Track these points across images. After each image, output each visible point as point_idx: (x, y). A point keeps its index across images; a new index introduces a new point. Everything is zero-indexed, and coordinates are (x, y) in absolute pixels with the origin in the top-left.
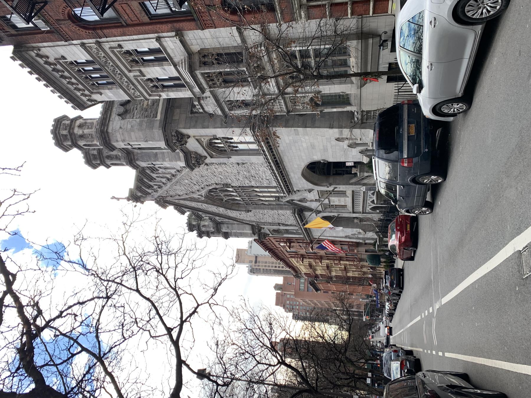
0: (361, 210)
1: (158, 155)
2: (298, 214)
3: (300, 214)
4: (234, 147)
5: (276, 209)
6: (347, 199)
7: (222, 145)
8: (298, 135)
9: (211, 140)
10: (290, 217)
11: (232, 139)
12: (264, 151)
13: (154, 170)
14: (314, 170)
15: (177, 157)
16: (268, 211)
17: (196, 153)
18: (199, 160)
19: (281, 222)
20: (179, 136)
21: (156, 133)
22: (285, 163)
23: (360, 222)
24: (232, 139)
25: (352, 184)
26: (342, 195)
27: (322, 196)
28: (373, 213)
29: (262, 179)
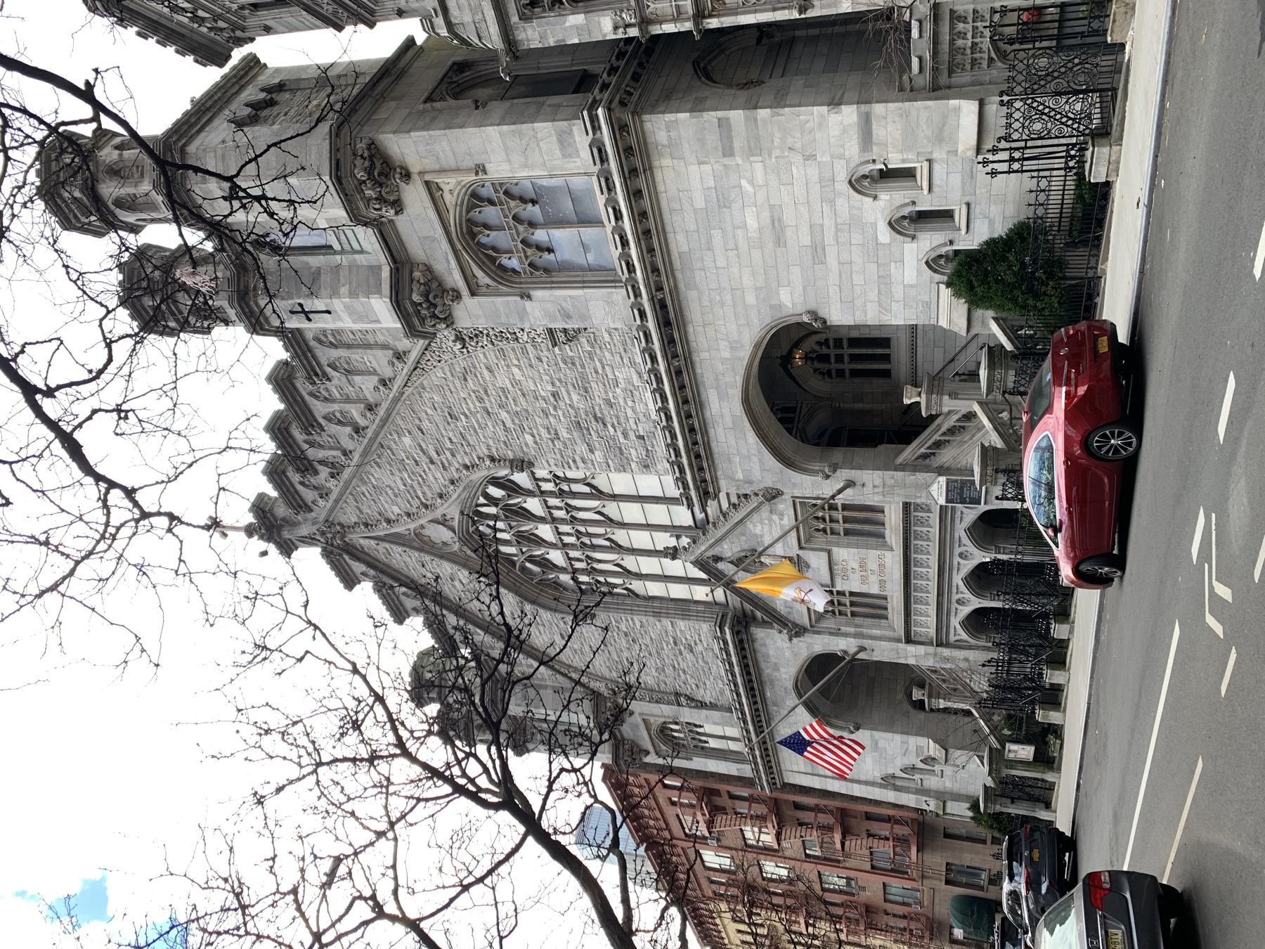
0: (932, 632)
1: (323, 277)
2: (731, 629)
3: (738, 633)
4: (700, 741)
5: (667, 615)
6: (888, 554)
7: (682, 735)
8: (732, 154)
9: (665, 723)
10: (709, 657)
11: (700, 726)
12: (754, 757)
13: (317, 375)
14: (790, 426)
15: (372, 281)
16: (644, 619)
17: (428, 269)
18: (435, 297)
19: (683, 691)
20: (378, 165)
21: (314, 150)
22: (690, 329)
23: (930, 696)
24: (700, 726)
25: (902, 468)
26: (872, 541)
27: (808, 541)
28: (970, 648)
29: (625, 435)
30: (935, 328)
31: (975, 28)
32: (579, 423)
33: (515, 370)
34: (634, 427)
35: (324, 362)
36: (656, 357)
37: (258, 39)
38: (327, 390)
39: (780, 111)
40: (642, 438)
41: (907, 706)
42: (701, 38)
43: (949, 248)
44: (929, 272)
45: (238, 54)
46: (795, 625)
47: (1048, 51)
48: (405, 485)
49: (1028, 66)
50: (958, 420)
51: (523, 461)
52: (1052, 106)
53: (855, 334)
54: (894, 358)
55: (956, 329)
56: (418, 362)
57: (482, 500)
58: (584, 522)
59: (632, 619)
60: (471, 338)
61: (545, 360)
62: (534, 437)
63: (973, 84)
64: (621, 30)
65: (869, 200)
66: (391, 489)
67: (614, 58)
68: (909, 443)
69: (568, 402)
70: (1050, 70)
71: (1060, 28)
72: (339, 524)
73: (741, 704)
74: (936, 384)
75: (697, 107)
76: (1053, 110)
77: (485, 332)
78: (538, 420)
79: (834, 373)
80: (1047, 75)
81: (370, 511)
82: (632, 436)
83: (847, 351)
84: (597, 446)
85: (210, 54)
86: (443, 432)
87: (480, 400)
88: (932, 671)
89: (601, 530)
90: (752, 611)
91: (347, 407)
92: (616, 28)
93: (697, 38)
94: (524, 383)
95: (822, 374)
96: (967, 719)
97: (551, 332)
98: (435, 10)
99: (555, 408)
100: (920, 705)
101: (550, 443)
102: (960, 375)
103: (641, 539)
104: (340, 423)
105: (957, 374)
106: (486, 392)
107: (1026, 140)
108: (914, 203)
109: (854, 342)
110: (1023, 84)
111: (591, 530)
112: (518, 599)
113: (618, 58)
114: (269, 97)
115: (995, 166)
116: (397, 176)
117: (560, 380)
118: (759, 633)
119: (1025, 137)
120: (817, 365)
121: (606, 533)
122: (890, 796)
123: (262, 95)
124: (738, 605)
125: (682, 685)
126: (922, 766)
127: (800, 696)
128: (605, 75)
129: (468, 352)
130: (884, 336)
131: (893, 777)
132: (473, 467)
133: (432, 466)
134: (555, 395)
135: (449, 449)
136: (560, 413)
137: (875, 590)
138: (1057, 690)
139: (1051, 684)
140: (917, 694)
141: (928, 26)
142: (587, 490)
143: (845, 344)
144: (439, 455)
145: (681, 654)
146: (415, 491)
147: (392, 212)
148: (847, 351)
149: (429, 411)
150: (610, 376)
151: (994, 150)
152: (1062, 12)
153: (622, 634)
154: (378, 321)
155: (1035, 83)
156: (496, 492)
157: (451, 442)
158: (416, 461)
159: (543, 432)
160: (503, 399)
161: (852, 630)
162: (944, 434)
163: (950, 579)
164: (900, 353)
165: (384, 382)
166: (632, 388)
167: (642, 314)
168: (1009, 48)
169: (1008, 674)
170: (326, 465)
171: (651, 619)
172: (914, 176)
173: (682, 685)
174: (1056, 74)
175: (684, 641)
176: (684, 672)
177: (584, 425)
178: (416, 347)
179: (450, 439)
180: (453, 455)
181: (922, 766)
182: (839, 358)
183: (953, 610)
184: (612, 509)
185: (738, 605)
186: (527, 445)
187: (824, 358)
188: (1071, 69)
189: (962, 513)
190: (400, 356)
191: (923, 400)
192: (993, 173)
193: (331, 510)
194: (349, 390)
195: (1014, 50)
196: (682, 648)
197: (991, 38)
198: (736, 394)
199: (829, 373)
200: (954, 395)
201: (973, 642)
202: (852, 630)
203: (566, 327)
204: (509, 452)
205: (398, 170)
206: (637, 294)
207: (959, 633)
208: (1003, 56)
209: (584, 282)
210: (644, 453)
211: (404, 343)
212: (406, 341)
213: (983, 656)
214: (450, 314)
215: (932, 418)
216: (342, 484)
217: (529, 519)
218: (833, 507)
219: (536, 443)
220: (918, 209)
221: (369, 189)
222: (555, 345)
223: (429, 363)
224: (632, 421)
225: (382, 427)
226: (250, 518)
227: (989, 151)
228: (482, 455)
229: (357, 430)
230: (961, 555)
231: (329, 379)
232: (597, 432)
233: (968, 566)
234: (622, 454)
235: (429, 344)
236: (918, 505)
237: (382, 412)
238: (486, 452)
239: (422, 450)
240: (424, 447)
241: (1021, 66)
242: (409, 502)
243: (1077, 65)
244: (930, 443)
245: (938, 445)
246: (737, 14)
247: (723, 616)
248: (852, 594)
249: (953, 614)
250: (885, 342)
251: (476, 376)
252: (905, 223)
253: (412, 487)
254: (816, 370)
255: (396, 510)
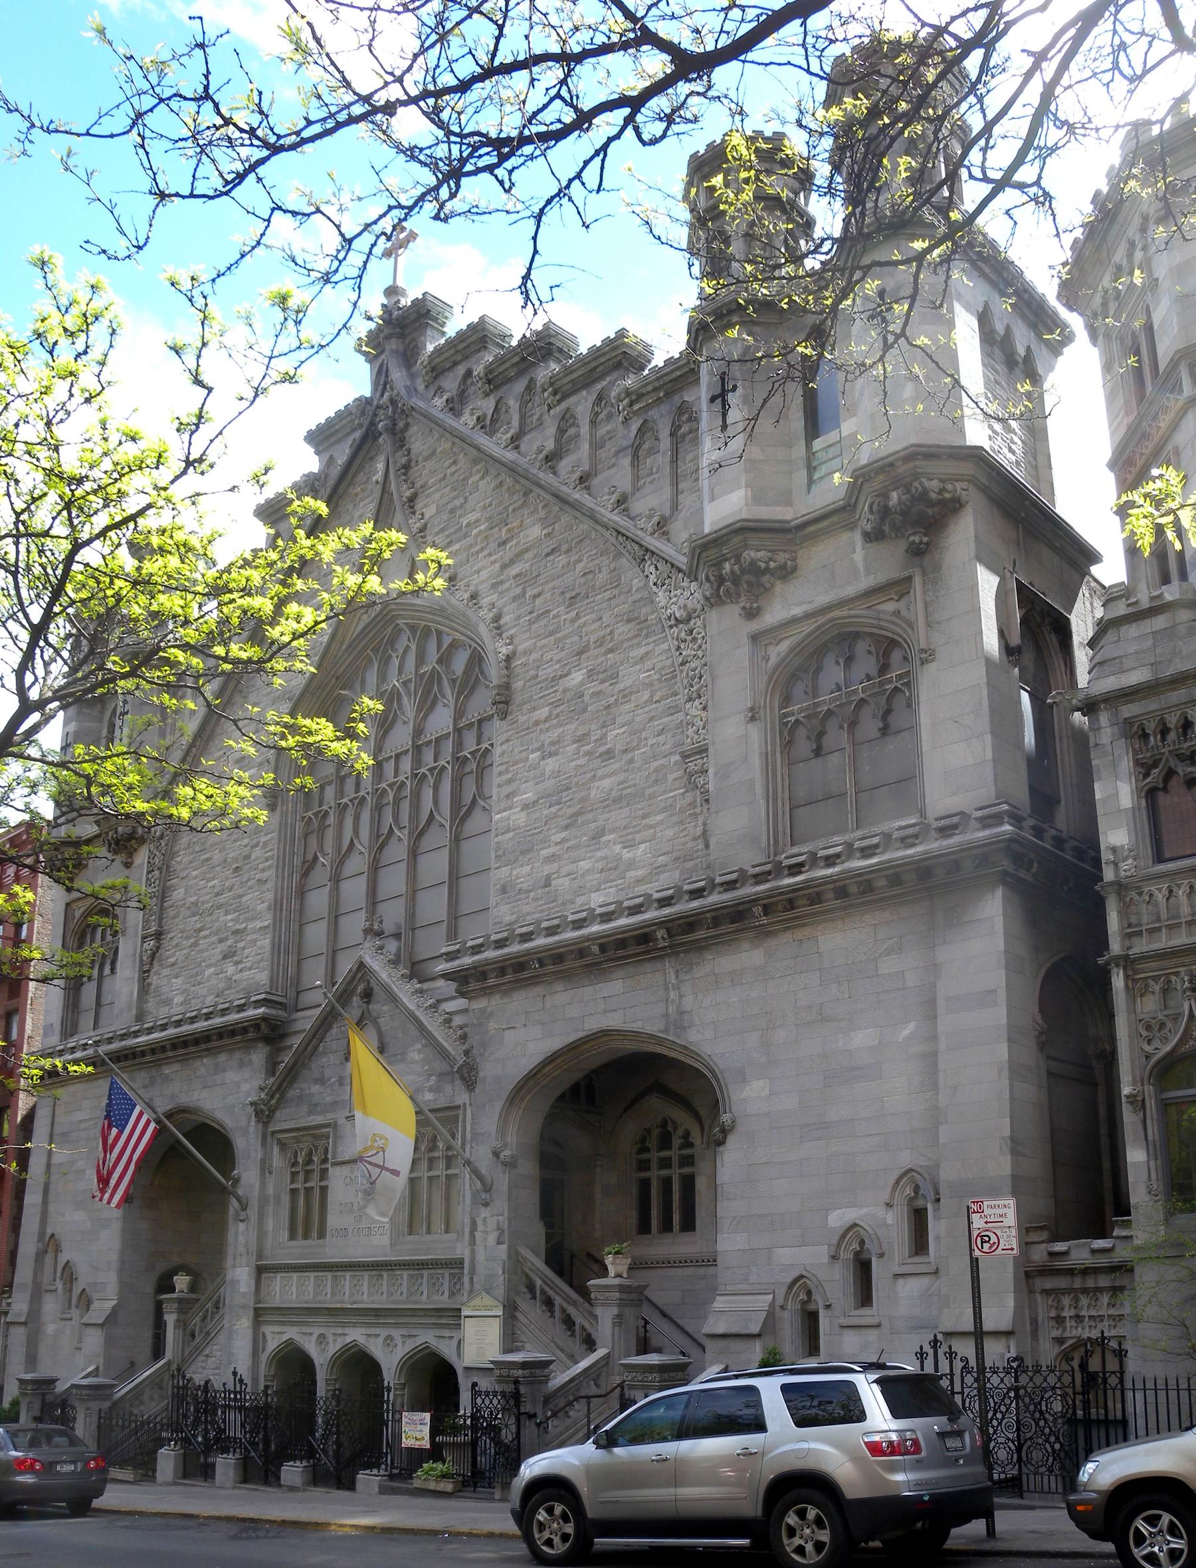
0: (276, 1302)
2: (264, 1018)
5: (277, 921)
6: (385, 1240)
16: (270, 885)
23: (180, 1301)
28: (255, 1354)
30: (713, 1291)
31: (1101, 1318)
32: (568, 789)
33: (646, 695)
34: (564, 871)
35: (653, 413)
36: (669, 905)
37: (1096, 350)
38: (610, 416)
39: (1006, 1073)
40: (547, 884)
41: (162, 1267)
42: (1100, 966)
43: (821, 1305)
44: (789, 1280)
45: (1075, 321)
46: (273, 1111)
47: (1071, 1411)
48: (468, 525)
49: (1054, 1388)
50: (583, 1328)
51: (507, 703)
52: (1004, 1422)
53: (701, 1184)
54: (667, 1238)
55: (711, 1319)
56: (653, 553)
57: (447, 641)
58: (416, 797)
59: (270, 867)
60: (691, 631)
61: (662, 738)
62: (546, 721)
63: (1034, 1322)
64: (1112, 857)
65: (885, 1195)
66: (462, 506)
67: (1076, 843)
68: (547, 1263)
69: (599, 773)
70: (1047, 1416)
71: (1098, 1421)
72: (407, 425)
73: (150, 1031)
74: (634, 1296)
75: (1012, 965)
76: (1000, 1424)
77: (700, 653)
78: (573, 726)
79: (644, 1156)
80: (1041, 1412)
81: (424, 473)
82: (548, 869)
83: (675, 1173)
84: (537, 815)
85: (1070, 291)
86: (551, 585)
87: (600, 642)
88: (218, 1302)
89: (405, 819)
90: (291, 1047)
91: (585, 447)
92: (1114, 850)
93: (1101, 961)
94: (626, 707)
95: (643, 1140)
96: (148, 1351)
97: (703, 751)
98: (1136, 603)
99: (588, 753)
100: (165, 1285)
101: (536, 745)
102: (645, 1327)
103: (394, 881)
104: (561, 431)
105: (646, 1322)
106: (611, 651)
107: (962, 1393)
108: (881, 1255)
109: (689, 1184)
110: (1031, 1384)
111: (405, 806)
112: (298, 692)
113: (1075, 849)
114: (1020, 360)
115: (931, 1358)
116: (917, 539)
117: (631, 761)
118: (259, 1056)
119: (966, 1391)
120: (655, 1133)
121: (400, 828)
122: (28, 1246)
123: (1021, 351)
124: (299, 1026)
125: (175, 942)
126: (76, 1291)
127: (169, 1115)
128: (1053, 832)
129: (671, 627)
130: (698, 1223)
131: (58, 1250)
132: (497, 628)
133: (497, 566)
134: (609, 754)
135: (524, 592)
136: (582, 761)
137: (332, 1221)
138: (207, 1472)
139: (213, 1465)
140: (181, 1282)
141: (1103, 1261)
142: (467, 799)
143: (686, 1170)
144: (515, 577)
145: (221, 941)
146: (459, 540)
147: (868, 527)
148: (675, 1173)
149: (579, 567)
150: (638, 837)
151: (951, 1355)
152: (1116, 1422)
153: (246, 851)
154: (712, 499)
155: (1032, 1399)
156: (460, 662)
157: (535, 597)
158: (504, 543)
159: (554, 734)
160: (601, 676)
161: (270, 1191)
162: (563, 1310)
163: (355, 1325)
164: (680, 1246)
165: (622, 501)
166: (622, 868)
167: (730, 885)
168: (1076, 1363)
169: (225, 1406)
170: (496, 410)
171: (270, 896)
172: (917, 1254)
173: (175, 942)
174: (1042, 1423)
175: (241, 945)
176: (196, 944)
177: (565, 795)
178: (676, 550)
179: (539, 594)
180: (515, 599)
181: (76, 1291)
182: (665, 1163)
183: (309, 1330)
184: (438, 837)
185: (299, 1026)
186: (534, 709)
187: (665, 1141)
188: (1047, 1441)
189: (451, 1338)
190: (662, 527)
191: (610, 1281)
192: (922, 1355)
193: (428, 417)
194: (611, 447)
195: (1073, 1370)
196: (229, 943)
197: (1089, 1339)
198: (614, 1021)
199: (644, 1149)
200: (619, 1320)
201: (264, 1358)
202: (270, 1191)
203: (711, 772)
204: (521, 683)
205: (925, 539)
206: (759, 878)
207: (275, 1337)
208: (1066, 1356)
209: (775, 800)
210: (524, 886)
211: (681, 533)
212: (684, 535)
213: (244, 1370)
214: (724, 603)
215: (584, 1293)
216: (469, 432)
217: (419, 710)
218: (449, 1161)
219: (537, 723)
220: (874, 1261)
221: (899, 498)
222: (685, 756)
223: (652, 569)
224: (572, 867)
225: (556, 496)
226: (412, 294)
227: (950, 1347)
228: (515, 642)
229: (551, 459)
230: (389, 1338)
231: (626, 420)
232: (555, 816)
233: (376, 1349)
234: (523, 853)
235: (680, 570)
236: (460, 1279)
237: (577, 495)
238: (521, 648)
239: (522, 553)
240: (526, 556)
241: (1052, 1380)
242: (442, 530)
243: (1052, 1447)
244: (551, 1293)
245: (549, 1303)
246: (1129, 1012)
247: (280, 1004)
248: (324, 1189)
249: (304, 1329)
250: (689, 1225)
251: (635, 636)
252: (855, 1246)
253: (466, 536)
254: (648, 1131)
255: (430, 511)
